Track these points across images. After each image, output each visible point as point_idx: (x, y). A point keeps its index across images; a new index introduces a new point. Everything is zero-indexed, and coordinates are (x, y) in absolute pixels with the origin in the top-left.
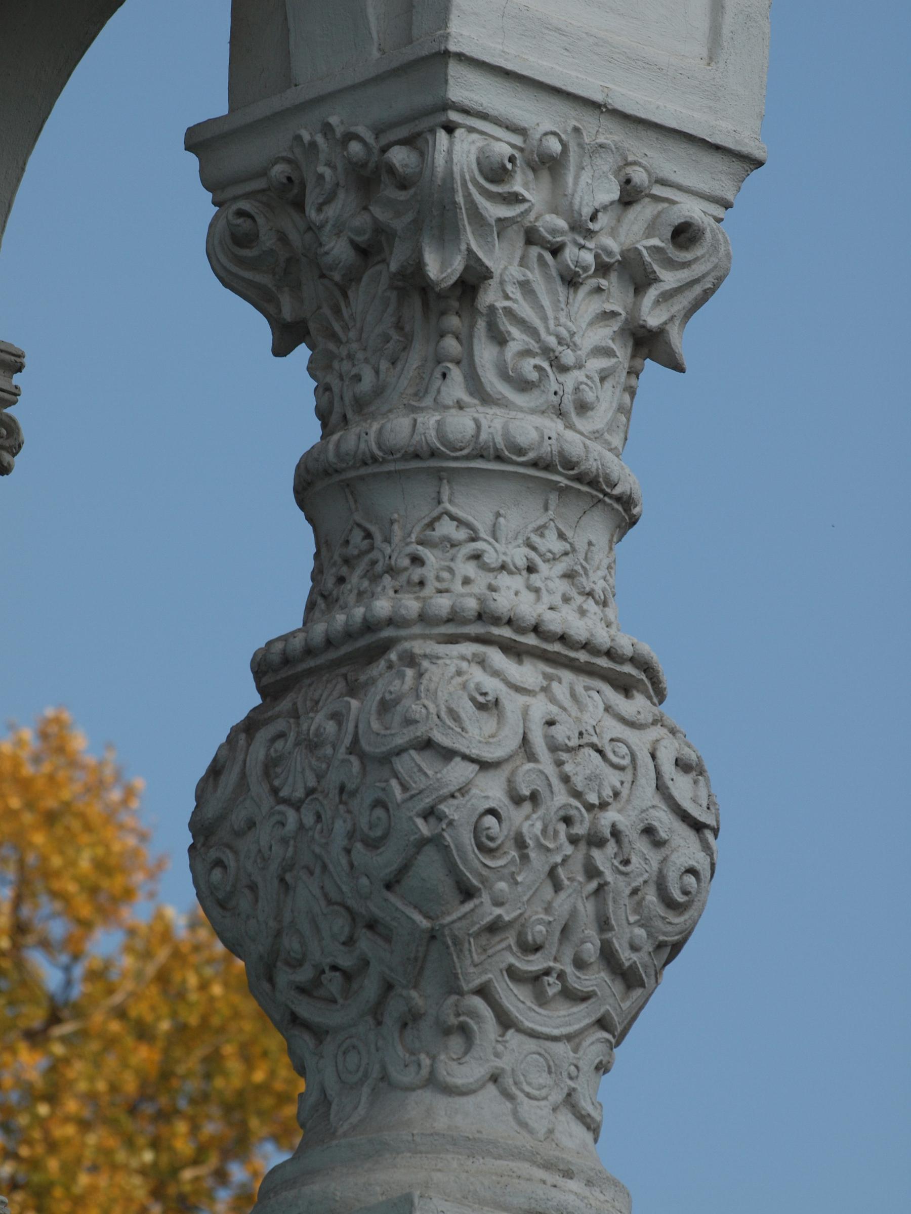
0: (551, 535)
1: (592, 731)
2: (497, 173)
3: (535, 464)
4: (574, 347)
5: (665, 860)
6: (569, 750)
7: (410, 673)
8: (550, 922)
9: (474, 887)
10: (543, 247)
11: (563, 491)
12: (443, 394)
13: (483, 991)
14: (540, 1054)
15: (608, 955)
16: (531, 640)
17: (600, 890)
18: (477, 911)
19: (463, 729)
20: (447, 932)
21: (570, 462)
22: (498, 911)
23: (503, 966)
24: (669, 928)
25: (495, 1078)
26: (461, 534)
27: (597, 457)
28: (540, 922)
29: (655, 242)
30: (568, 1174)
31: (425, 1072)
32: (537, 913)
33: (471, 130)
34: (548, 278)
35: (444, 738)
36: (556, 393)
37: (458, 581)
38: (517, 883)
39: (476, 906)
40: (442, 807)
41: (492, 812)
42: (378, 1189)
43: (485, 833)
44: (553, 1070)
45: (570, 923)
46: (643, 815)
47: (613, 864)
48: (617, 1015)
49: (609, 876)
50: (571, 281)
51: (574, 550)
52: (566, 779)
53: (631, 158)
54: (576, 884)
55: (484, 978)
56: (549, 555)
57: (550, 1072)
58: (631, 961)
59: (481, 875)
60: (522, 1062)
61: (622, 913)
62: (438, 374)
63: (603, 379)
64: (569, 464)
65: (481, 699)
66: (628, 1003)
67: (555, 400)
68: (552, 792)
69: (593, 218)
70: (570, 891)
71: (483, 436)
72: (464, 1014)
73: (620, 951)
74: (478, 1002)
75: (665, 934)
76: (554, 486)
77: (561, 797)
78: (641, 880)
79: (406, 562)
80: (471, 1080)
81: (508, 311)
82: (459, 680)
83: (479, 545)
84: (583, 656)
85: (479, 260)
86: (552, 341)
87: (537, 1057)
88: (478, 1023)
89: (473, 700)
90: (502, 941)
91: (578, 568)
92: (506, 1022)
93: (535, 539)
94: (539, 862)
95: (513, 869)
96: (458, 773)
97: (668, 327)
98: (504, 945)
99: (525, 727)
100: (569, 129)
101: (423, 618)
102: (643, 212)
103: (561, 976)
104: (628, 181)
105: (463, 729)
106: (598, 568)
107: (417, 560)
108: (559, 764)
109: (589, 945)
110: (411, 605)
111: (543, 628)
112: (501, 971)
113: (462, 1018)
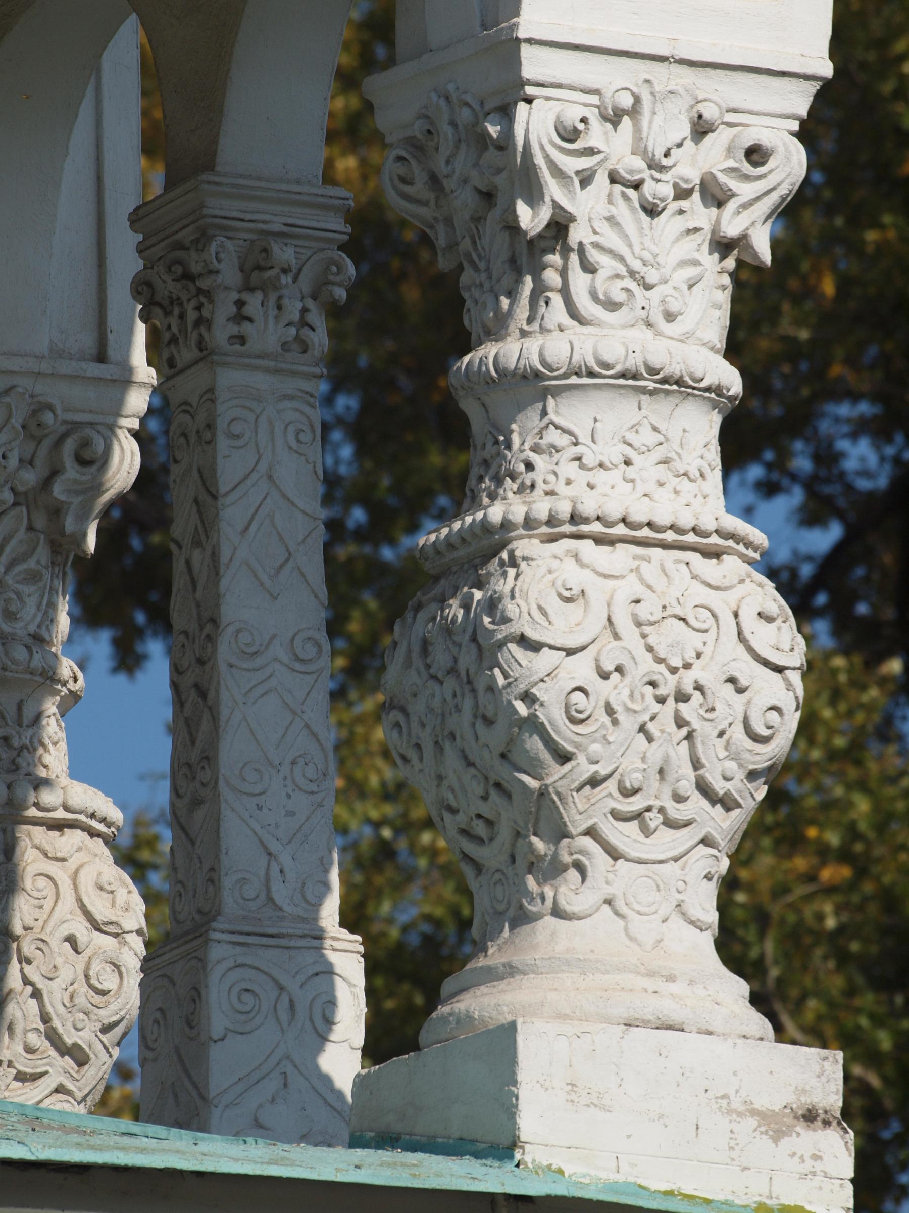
0: (646, 430)
1: (675, 603)
2: (569, 135)
3: (623, 375)
4: (657, 266)
5: (749, 702)
6: (652, 624)
7: (512, 572)
8: (645, 769)
9: (569, 752)
10: (624, 185)
11: (652, 393)
12: (546, 319)
13: (591, 832)
14: (648, 877)
15: (703, 788)
16: (620, 530)
17: (689, 737)
18: (575, 770)
19: (550, 623)
20: (551, 790)
21: (654, 369)
22: (594, 768)
23: (607, 810)
24: (758, 758)
25: (608, 902)
26: (562, 440)
27: (680, 361)
28: (636, 770)
29: (731, 163)
30: (671, 978)
31: (549, 903)
32: (633, 763)
33: (548, 98)
34: (632, 209)
35: (533, 632)
36: (643, 308)
37: (562, 481)
38: (609, 743)
39: (573, 767)
40: (534, 691)
41: (579, 689)
42: (505, 1008)
43: (573, 708)
44: (662, 887)
45: (665, 767)
46: (725, 668)
47: (699, 714)
48: (719, 834)
49: (696, 724)
50: (652, 211)
51: (667, 440)
52: (650, 649)
53: (700, 98)
54: (665, 735)
55: (590, 823)
56: (644, 449)
57: (659, 890)
58: (725, 790)
59: (574, 742)
60: (631, 886)
61: (713, 753)
62: (543, 304)
63: (690, 287)
64: (653, 371)
65: (567, 594)
66: (728, 823)
67: (643, 314)
68: (636, 663)
69: (666, 155)
70: (661, 741)
71: (576, 358)
72: (576, 853)
73: (713, 782)
74: (587, 842)
75: (754, 763)
76: (644, 390)
77: (647, 664)
78: (726, 723)
79: (522, 467)
80: (587, 907)
81: (596, 245)
82: (550, 577)
83: (579, 449)
84: (670, 536)
85: (562, 208)
86: (636, 265)
87: (646, 879)
88: (589, 859)
89: (560, 596)
90: (602, 790)
91: (673, 455)
92: (614, 854)
93: (631, 437)
94: (628, 723)
95: (604, 732)
96: (545, 660)
97: (749, 232)
98: (604, 793)
99: (609, 611)
100: (640, 82)
101: (529, 523)
102: (716, 142)
103: (661, 810)
104: (700, 117)
105: (550, 623)
106: (694, 450)
107: (529, 466)
108: (644, 636)
109: (684, 783)
110: (518, 511)
111: (629, 520)
112: (605, 814)
113: (575, 856)
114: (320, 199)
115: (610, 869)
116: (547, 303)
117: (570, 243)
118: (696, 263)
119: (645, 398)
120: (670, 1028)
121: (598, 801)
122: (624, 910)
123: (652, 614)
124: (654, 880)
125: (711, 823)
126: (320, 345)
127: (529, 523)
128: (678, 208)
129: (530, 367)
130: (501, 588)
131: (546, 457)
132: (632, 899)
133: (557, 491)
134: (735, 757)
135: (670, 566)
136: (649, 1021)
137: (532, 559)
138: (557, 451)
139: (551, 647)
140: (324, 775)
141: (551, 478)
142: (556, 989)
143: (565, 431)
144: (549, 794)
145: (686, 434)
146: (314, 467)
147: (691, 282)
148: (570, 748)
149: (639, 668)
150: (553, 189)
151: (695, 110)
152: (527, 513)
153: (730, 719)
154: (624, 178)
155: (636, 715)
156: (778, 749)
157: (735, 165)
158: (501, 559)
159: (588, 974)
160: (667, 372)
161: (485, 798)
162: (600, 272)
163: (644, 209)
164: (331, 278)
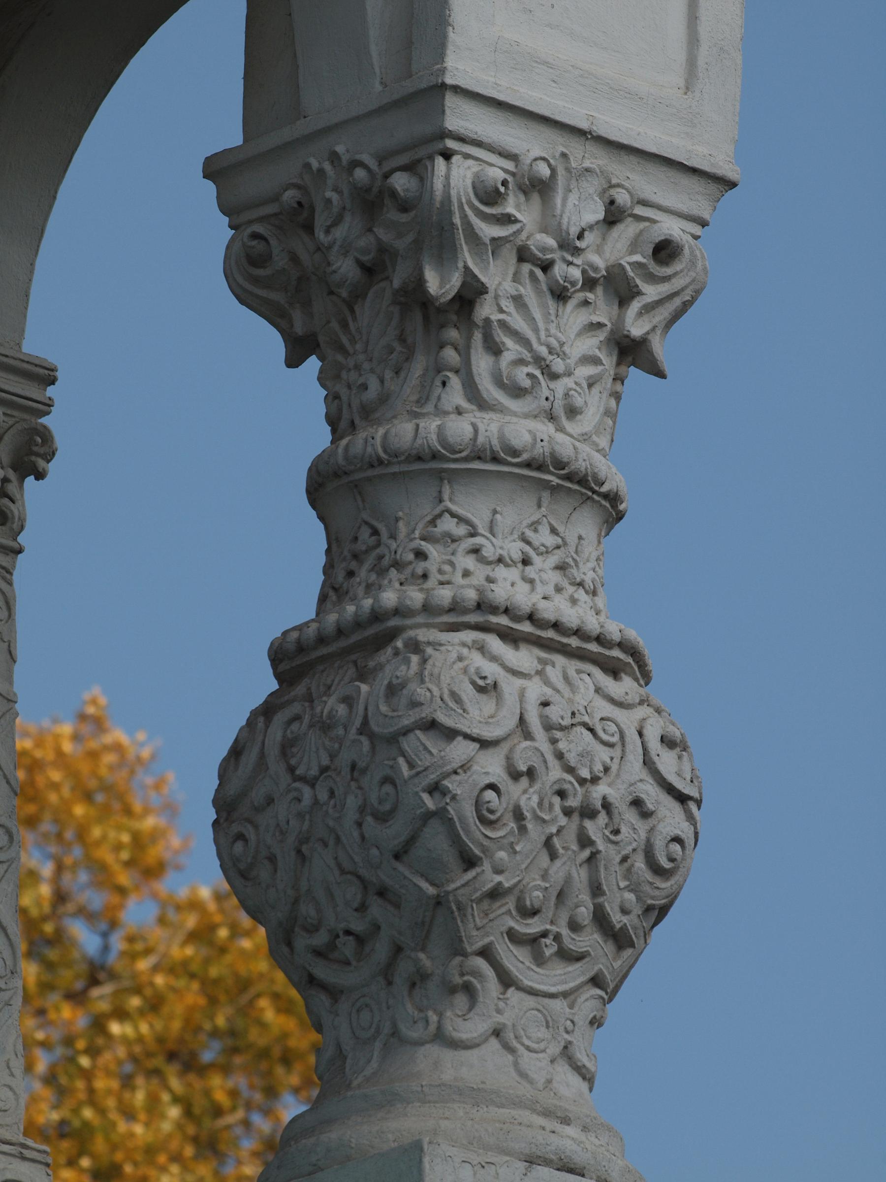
0: (544, 530)
1: (583, 711)
3: (528, 465)
4: (563, 356)
6: (562, 728)
7: (415, 659)
9: (476, 856)
11: (555, 490)
12: (443, 400)
13: (485, 953)
14: (538, 1010)
15: (601, 919)
16: (526, 627)
17: (592, 858)
19: (464, 711)
20: (451, 898)
21: (561, 462)
22: (498, 878)
23: (504, 929)
24: (657, 893)
25: (497, 1033)
26: (461, 530)
27: (586, 458)
28: (537, 888)
30: (566, 1121)
31: (432, 1027)
32: (534, 880)
33: (467, 156)
34: (539, 292)
35: (447, 718)
37: (459, 574)
38: (515, 852)
39: (478, 874)
40: (446, 782)
42: (390, 1136)
48: (609, 973)
49: (601, 845)
50: (560, 295)
51: (565, 544)
52: (560, 756)
54: (570, 852)
55: (487, 940)
56: (543, 549)
58: (622, 924)
59: (482, 845)
60: (522, 1018)
62: (438, 383)
63: (590, 386)
65: (481, 683)
66: (619, 963)
67: (547, 405)
68: (547, 768)
69: (580, 236)
71: (481, 439)
73: (611, 913)
74: (481, 963)
75: (653, 898)
77: (556, 773)
78: (630, 848)
79: (411, 556)
80: (475, 1035)
81: (503, 324)
82: (461, 665)
83: (478, 540)
84: (574, 642)
86: (543, 351)
87: (536, 1012)
88: (481, 982)
89: (473, 683)
91: (569, 561)
92: (507, 981)
93: (529, 534)
95: (512, 839)
96: (460, 750)
97: (650, 337)
98: (503, 910)
99: (521, 708)
100: (557, 155)
101: (427, 608)
102: (626, 231)
103: (557, 938)
104: (612, 202)
105: (464, 711)
106: (588, 561)
107: (421, 555)
109: (583, 909)
110: (415, 596)
112: (502, 933)
113: (466, 978)
114: (25, 366)
115: (501, 996)
116: (444, 384)
117: (475, 319)
118: (596, 361)
119: (546, 495)
120: (571, 1171)
121: (496, 918)
122: (515, 1044)
123: (562, 718)
124: (544, 1015)
125: (604, 960)
126: (19, 518)
127: (427, 608)
128: (583, 299)
129: (429, 447)
130: (403, 673)
131: (439, 547)
132: (522, 1033)
133: (453, 580)
134: (633, 888)
135: (572, 673)
136: (551, 1161)
137: (441, 645)
138: (453, 541)
139: (467, 736)
140: (12, 973)
141: (447, 568)
142: (447, 1118)
143: (461, 519)
144: (448, 901)
145: (582, 542)
146: (9, 646)
147: (591, 381)
148: (477, 851)
149: (550, 774)
150: (467, 257)
151: (607, 195)
152: (426, 599)
153: (634, 845)
154: (534, 255)
155: (544, 826)
156: (676, 886)
157: (644, 261)
158: (396, 648)
159: (481, 1105)
160: (573, 467)
161: (362, 908)
162: (505, 354)
163: (552, 292)
164: (35, 449)
